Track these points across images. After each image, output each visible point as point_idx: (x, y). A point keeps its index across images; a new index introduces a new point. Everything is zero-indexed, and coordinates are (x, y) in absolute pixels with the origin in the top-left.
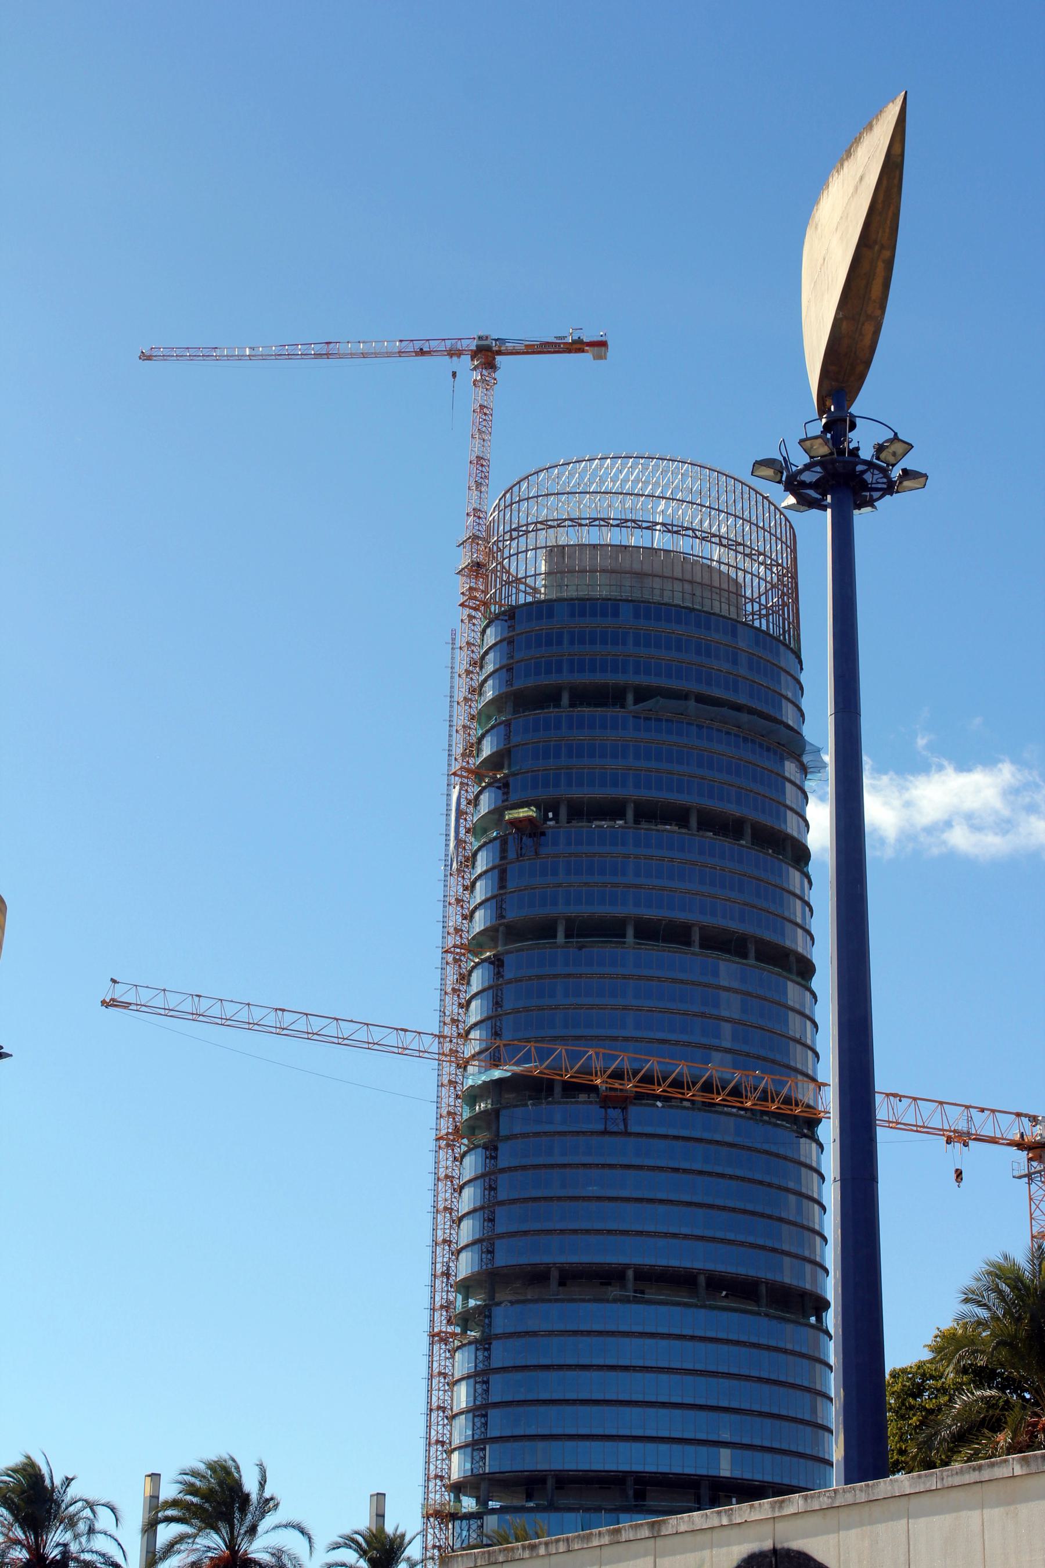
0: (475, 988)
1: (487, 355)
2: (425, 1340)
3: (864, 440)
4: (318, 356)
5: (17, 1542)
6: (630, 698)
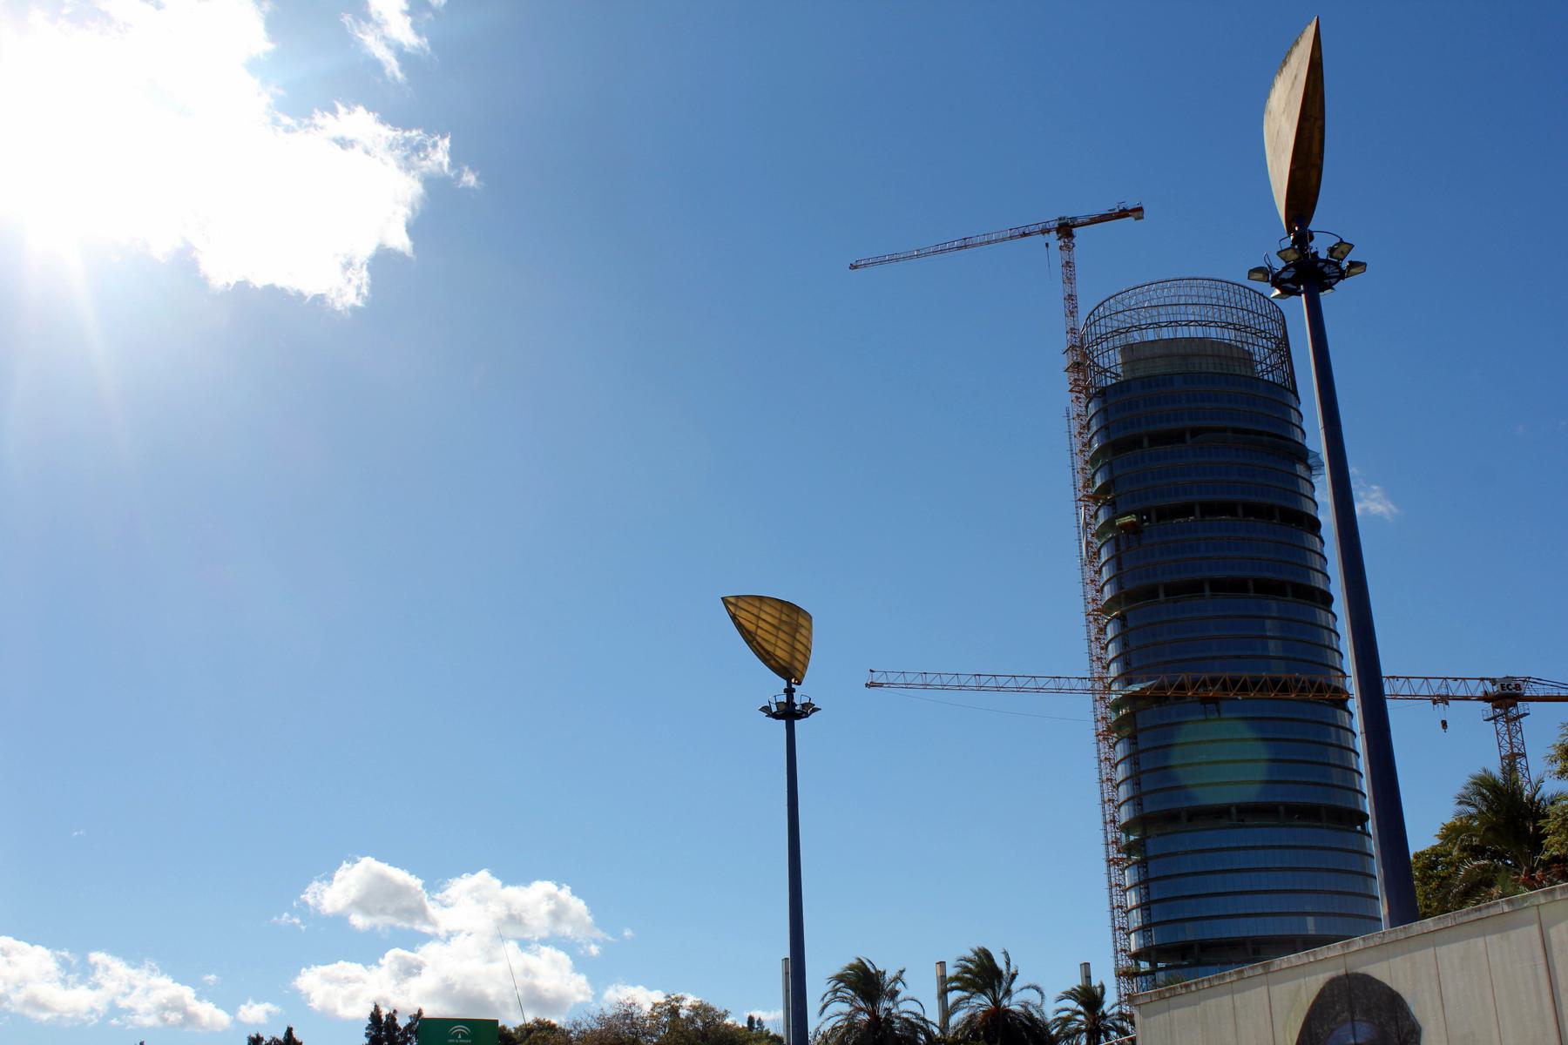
0: (1110, 636)
1: (1066, 229)
2: (1104, 864)
3: (1320, 246)
4: (959, 248)
5: (861, 1009)
6: (1188, 436)
